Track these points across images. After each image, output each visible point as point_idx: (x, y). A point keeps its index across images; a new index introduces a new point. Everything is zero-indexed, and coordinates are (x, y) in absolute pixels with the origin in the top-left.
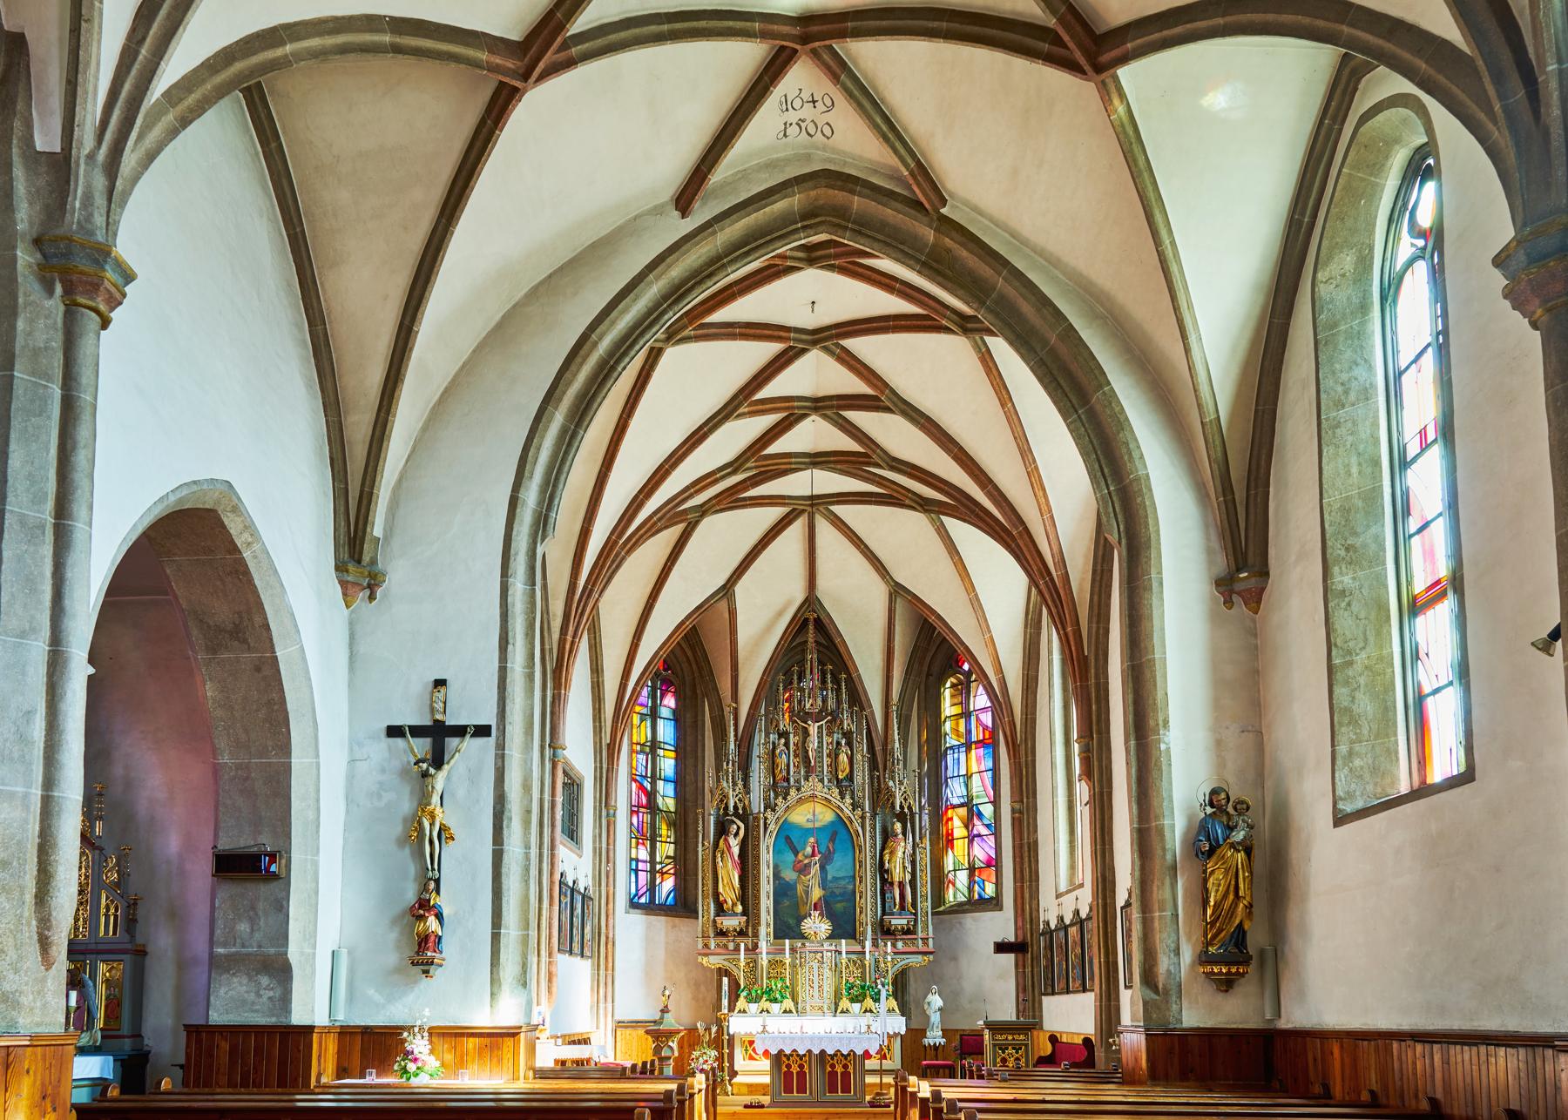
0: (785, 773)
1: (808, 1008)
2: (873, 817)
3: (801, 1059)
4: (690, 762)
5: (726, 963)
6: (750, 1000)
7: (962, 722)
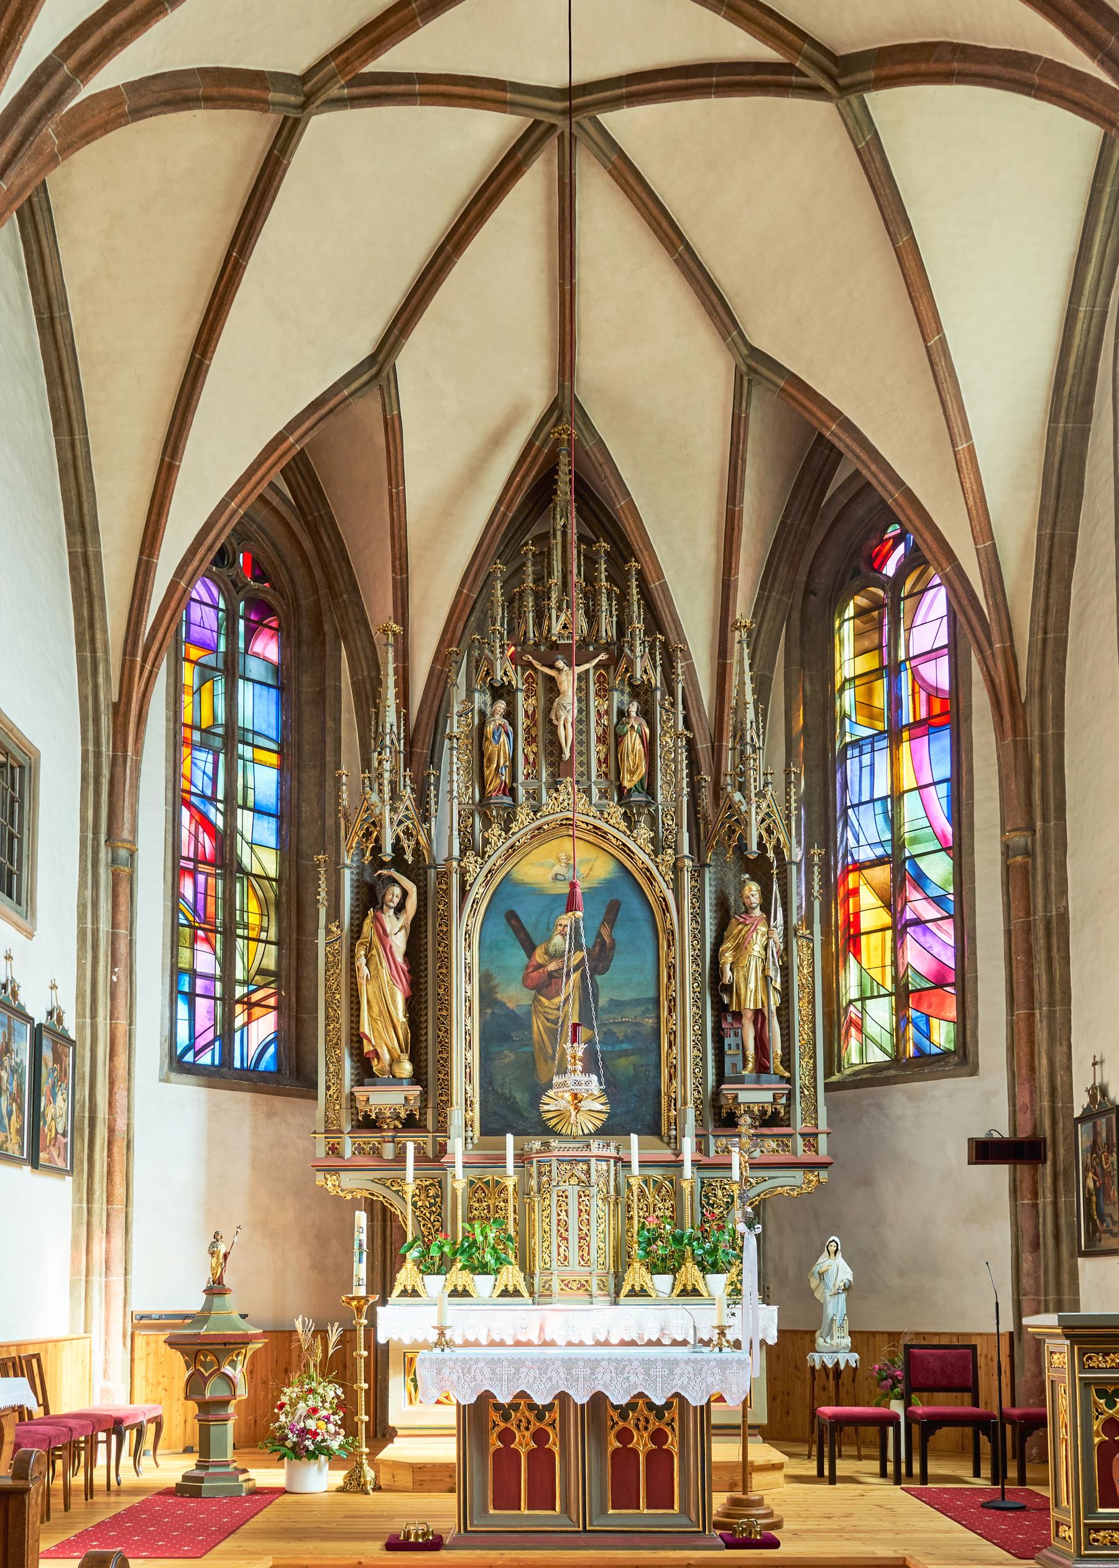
0: (505, 777)
1: (556, 1285)
2: (698, 873)
3: (540, 1417)
4: (310, 775)
5: (377, 1189)
6: (427, 1267)
7: (881, 687)
